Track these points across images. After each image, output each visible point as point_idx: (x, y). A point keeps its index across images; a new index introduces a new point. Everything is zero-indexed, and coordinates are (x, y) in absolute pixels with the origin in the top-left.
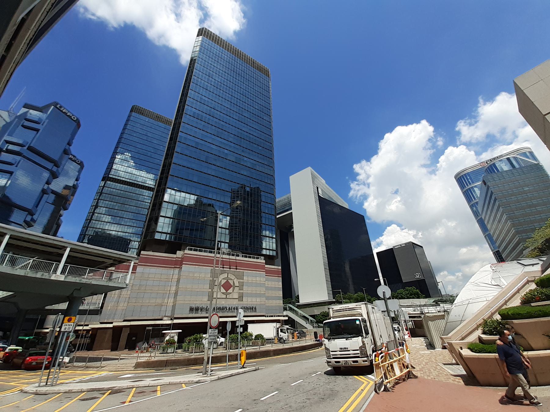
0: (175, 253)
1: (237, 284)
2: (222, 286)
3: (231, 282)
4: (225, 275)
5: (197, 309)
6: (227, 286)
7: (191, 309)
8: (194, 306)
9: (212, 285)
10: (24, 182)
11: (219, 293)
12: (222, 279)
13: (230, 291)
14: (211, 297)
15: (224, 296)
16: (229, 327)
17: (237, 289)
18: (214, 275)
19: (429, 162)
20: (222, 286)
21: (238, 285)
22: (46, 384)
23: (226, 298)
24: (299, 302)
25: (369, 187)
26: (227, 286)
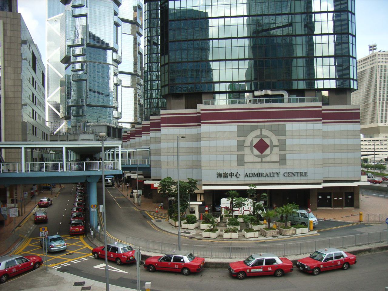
0: (151, 122)
1: (275, 143)
2: (254, 146)
3: (267, 141)
4: (257, 132)
5: (226, 176)
6: (262, 146)
7: (219, 175)
8: (221, 172)
9: (241, 146)
10: (221, 3)
11: (251, 155)
12: (252, 138)
13: (267, 152)
14: (241, 161)
15: (259, 160)
16: (299, 175)
17: (276, 150)
18: (242, 132)
19: (49, 269)
20: (254, 146)
21: (277, 144)
22: (356, 80)
23: (262, 162)
24: (316, 221)
25: (251, 100)
26: (262, 146)
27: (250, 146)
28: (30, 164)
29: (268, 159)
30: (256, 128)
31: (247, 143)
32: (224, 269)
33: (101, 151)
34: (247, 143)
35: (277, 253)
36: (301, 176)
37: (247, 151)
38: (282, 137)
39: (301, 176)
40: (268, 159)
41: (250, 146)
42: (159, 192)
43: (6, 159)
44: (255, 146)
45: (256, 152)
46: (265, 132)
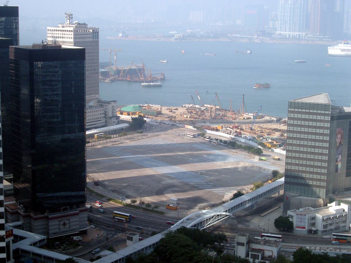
3: (66, 223)
4: (63, 221)
12: (62, 223)
17: (68, 225)
26: (64, 224)
27: (62, 225)
28: (251, 254)
29: (66, 227)
30: (62, 220)
31: (61, 224)
32: (116, 129)
33: (37, 244)
34: (61, 224)
35: (350, 155)
36: (217, 259)
37: (61, 226)
38: (69, 221)
39: (217, 259)
40: (66, 227)
41: (62, 225)
42: (287, 256)
43: (277, 182)
44: (66, 224)
45: (63, 226)
46: (65, 221)
